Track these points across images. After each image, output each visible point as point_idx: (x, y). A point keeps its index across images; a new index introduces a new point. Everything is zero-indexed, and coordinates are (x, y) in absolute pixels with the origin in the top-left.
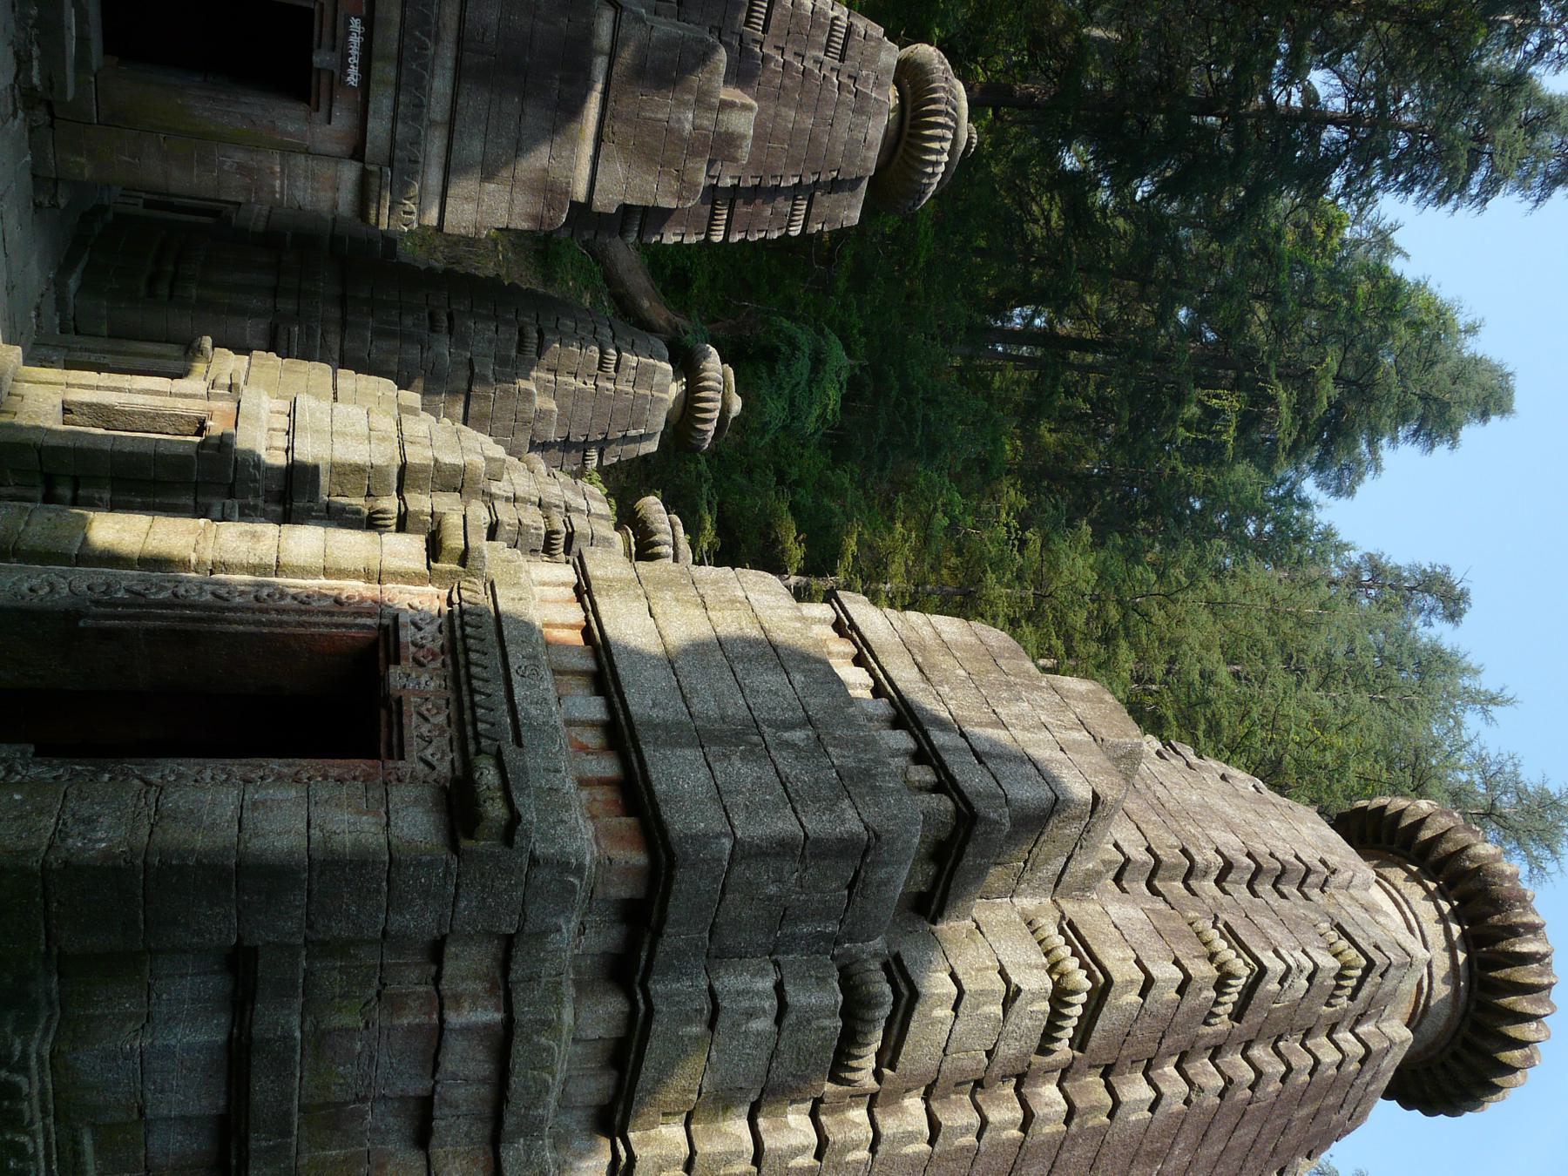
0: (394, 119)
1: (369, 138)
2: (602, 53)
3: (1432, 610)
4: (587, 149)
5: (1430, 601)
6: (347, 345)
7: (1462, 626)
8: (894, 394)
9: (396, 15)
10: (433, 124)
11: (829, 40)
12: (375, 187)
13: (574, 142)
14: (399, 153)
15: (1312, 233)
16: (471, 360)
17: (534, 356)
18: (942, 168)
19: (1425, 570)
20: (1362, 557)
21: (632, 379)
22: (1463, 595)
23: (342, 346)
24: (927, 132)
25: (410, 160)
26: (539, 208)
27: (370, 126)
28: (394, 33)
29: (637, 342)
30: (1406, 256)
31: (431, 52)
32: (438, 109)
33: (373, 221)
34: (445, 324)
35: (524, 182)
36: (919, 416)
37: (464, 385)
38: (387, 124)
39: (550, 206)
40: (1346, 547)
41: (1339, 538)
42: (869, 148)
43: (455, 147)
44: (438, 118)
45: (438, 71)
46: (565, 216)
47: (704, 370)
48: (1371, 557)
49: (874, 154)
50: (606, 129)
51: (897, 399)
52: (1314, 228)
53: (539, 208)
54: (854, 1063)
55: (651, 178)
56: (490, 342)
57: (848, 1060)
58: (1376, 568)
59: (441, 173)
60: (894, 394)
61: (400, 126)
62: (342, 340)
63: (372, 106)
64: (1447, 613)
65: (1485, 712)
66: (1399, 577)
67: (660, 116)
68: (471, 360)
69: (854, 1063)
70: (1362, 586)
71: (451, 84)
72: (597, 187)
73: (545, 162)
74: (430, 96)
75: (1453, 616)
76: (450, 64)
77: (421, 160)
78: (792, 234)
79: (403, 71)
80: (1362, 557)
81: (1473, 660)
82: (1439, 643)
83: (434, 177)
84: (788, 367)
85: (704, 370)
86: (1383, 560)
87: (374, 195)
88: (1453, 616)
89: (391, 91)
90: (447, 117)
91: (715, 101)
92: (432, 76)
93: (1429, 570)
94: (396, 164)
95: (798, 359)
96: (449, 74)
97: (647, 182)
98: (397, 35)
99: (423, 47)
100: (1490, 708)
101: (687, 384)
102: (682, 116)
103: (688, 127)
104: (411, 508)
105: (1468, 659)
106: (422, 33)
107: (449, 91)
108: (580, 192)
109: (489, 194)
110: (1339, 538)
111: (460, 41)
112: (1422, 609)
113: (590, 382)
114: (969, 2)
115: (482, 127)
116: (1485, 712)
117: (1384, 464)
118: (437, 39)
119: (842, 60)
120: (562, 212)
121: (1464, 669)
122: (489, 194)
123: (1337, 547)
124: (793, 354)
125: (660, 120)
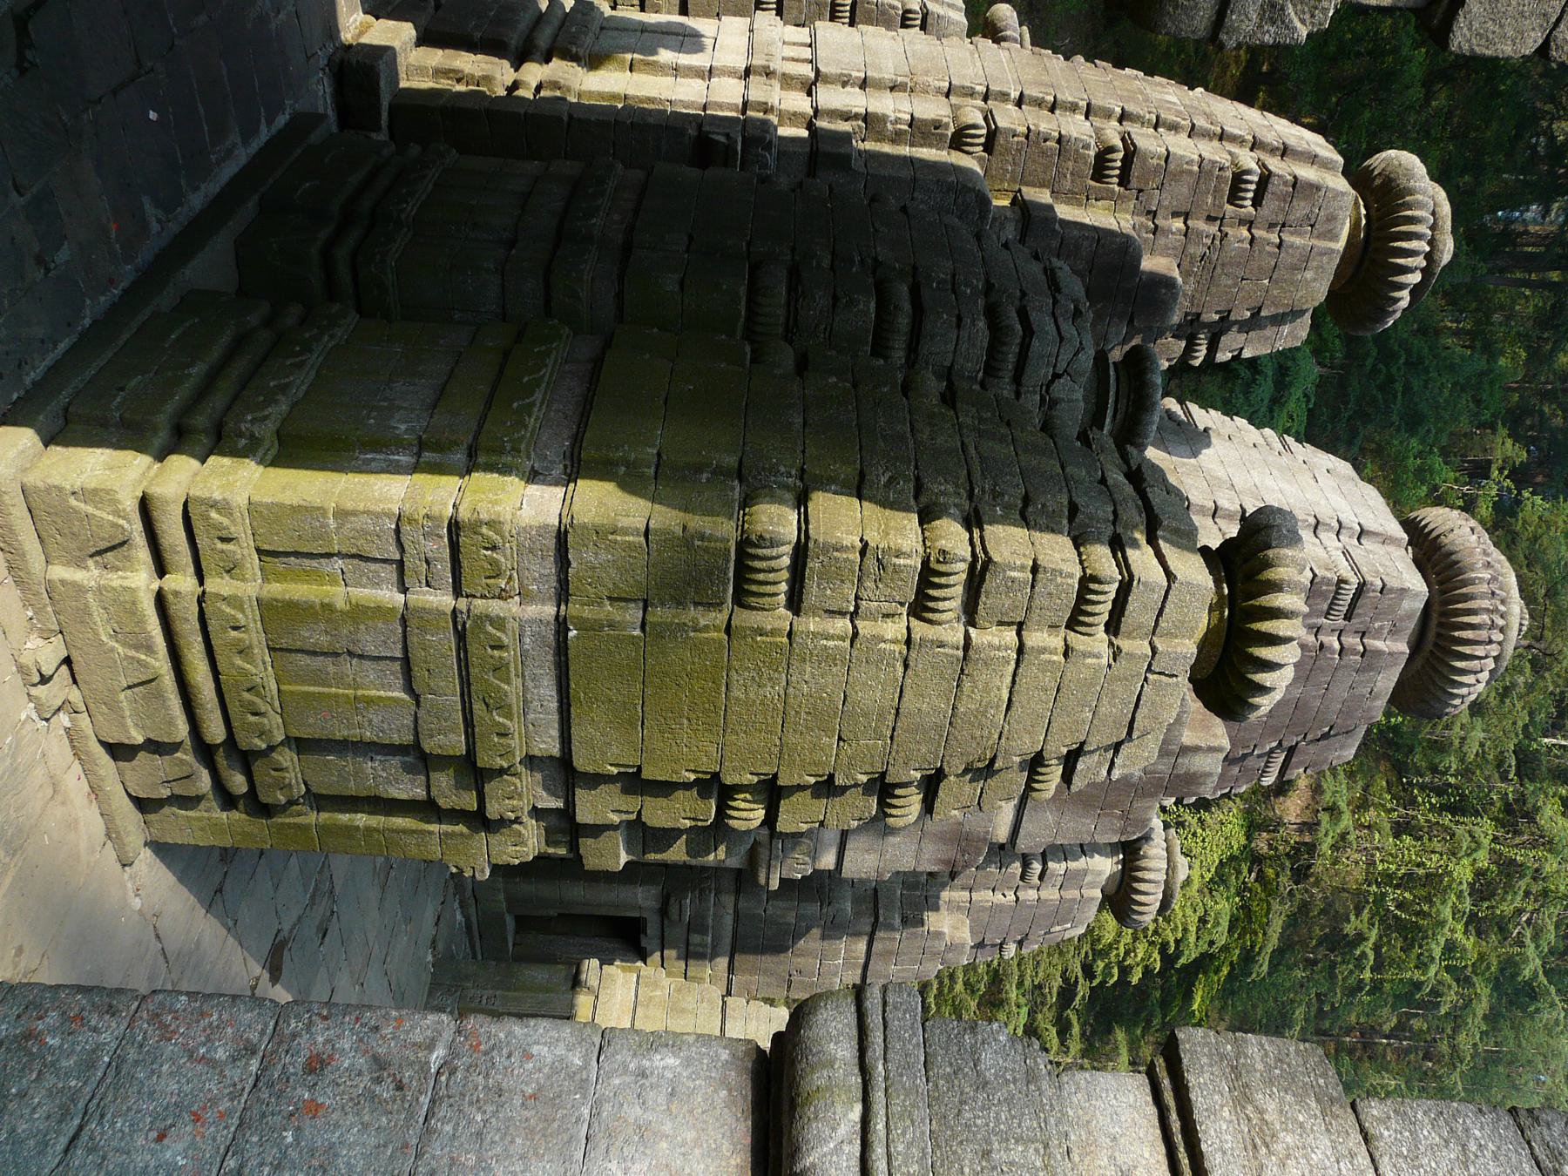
6: (740, 905)
8: (1369, 362)
11: (1330, 608)
17: (946, 879)
18: (1485, 676)
23: (736, 905)
24: (1456, 634)
33: (762, 881)
36: (1399, 387)
37: (868, 929)
42: (1376, 698)
47: (1144, 857)
51: (1374, 366)
60: (1369, 362)
62: (737, 900)
72: (1022, 832)
78: (1264, 784)
84: (1246, 393)
85: (1144, 857)
91: (1176, 748)
95: (1260, 385)
101: (1124, 862)
114: (1554, 728)
122: (894, 845)
124: (1254, 381)
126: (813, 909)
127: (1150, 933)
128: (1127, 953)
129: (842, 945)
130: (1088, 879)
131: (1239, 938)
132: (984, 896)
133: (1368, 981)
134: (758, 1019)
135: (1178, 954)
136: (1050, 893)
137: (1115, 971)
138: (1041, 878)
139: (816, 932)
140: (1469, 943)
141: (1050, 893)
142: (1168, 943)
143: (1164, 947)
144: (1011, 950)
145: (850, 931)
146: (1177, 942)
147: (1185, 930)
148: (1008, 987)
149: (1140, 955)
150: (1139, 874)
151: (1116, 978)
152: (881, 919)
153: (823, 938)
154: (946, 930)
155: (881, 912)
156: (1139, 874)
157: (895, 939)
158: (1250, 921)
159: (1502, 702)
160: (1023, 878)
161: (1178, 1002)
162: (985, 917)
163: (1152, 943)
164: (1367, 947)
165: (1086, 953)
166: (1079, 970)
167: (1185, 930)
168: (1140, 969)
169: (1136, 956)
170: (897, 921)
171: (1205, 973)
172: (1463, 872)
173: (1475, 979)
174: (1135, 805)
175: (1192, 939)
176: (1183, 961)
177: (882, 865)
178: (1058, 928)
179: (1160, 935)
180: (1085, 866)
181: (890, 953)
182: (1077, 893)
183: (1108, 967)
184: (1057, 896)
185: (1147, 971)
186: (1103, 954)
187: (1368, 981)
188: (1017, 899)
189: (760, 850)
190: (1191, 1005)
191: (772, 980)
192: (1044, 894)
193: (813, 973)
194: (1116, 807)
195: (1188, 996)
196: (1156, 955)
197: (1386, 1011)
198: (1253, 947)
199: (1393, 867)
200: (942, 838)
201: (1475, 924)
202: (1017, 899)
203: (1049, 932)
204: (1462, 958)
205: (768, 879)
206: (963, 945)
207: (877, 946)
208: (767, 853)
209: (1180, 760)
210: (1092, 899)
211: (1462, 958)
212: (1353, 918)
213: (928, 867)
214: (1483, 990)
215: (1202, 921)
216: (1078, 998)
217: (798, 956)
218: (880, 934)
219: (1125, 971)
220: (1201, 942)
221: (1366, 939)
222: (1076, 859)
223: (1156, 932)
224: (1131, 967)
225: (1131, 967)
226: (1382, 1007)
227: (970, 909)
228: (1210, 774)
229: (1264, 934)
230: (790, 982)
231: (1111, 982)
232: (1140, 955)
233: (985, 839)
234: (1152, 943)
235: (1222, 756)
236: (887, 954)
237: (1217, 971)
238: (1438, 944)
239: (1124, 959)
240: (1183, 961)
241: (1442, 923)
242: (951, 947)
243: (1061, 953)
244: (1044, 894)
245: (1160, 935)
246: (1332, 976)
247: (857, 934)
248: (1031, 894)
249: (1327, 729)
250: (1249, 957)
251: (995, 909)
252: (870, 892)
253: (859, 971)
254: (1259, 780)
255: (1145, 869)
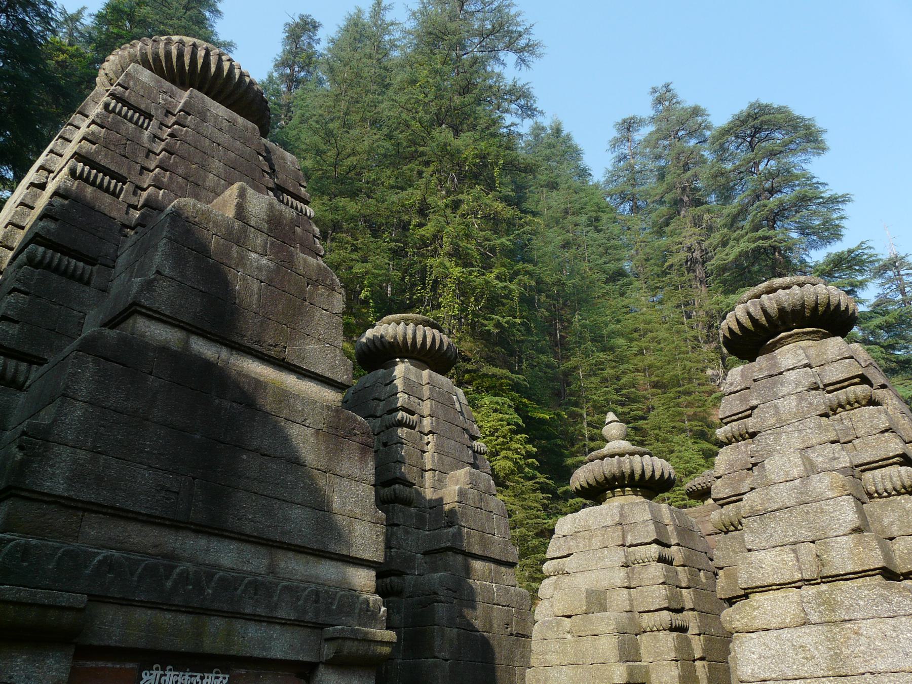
0: (271, 621)
1: (291, 656)
2: (187, 342)
3: (310, 38)
4: (291, 381)
5: (304, 38)
7: (322, 22)
9: (143, 616)
10: (272, 570)
12: (350, 647)
13: (284, 395)
14: (309, 617)
15: (62, 61)
16: (425, 554)
19: (287, 37)
20: (276, 71)
21: (417, 400)
22: (302, 18)
25: (317, 602)
26: (352, 447)
27: (279, 656)
28: (166, 619)
29: (377, 395)
30: (84, 8)
31: (192, 568)
32: (255, 562)
33: (386, 650)
34: (395, 579)
35: (330, 459)
37: (460, 558)
38: (276, 631)
39: (351, 434)
40: (270, 77)
41: (265, 80)
43: (299, 542)
44: (265, 562)
45: (211, 558)
46: (359, 418)
47: (395, 338)
48: (276, 66)
49: (240, 120)
50: (272, 353)
52: (60, 59)
53: (352, 447)
54: (747, 323)
55: (318, 314)
56: (407, 533)
57: (762, 326)
58: (283, 63)
59: (323, 562)
61: (281, 614)
63: (257, 653)
64: (312, 30)
65: (385, 9)
66: (290, 52)
67: (255, 288)
68: (425, 554)
69: (747, 323)
70: (293, 74)
71: (227, 542)
72: (328, 374)
73: (309, 431)
74: (245, 572)
75: (315, 26)
76: (203, 542)
77: (313, 587)
79: (216, 606)
80: (276, 71)
81: (353, 11)
82: (343, 27)
83: (328, 571)
85: (395, 338)
86: (279, 59)
87: (362, 648)
88: (315, 26)
89: (238, 625)
90: (263, 551)
91: (237, 224)
92: (219, 567)
93: (287, 34)
94: (322, 619)
96: (216, 544)
97: (321, 319)
98: (168, 616)
99: (184, 577)
100: (383, 5)
102: (255, 264)
103: (264, 261)
104: (880, 565)
105: (352, 14)
106: (167, 578)
107: (234, 546)
108: (331, 396)
109: (344, 504)
110: (265, 80)
111: (176, 525)
112: (309, 43)
113: (426, 439)
115: (277, 504)
116: (385, 9)
117: (229, 40)
118: (173, 557)
119: (149, 117)
120: (356, 420)
121: (358, 16)
122: (344, 504)
123: (270, 82)
125: (260, 289)
126: (441, 609)
127: (505, 440)
128: (518, 453)
129: (476, 583)
130: (412, 378)
131: (505, 393)
132: (429, 460)
133: (522, 320)
134: (545, 653)
135: (517, 424)
136: (426, 407)
137: (530, 460)
138: (412, 413)
139: (467, 612)
140: (496, 271)
141: (426, 407)
142: (510, 429)
143: (516, 432)
144: (479, 444)
145: (463, 574)
146: (509, 424)
147: (501, 420)
148: (546, 526)
149: (519, 446)
150: (409, 341)
151: (534, 460)
152: (449, 544)
153: (474, 608)
154: (457, 487)
155: (443, 545)
156: (409, 341)
157: (467, 532)
158: (495, 387)
159: (360, 249)
160: (413, 427)
161: (546, 427)
162: (447, 460)
163: (511, 439)
164: (503, 321)
165: (520, 477)
166: (531, 483)
167: (501, 420)
168: (527, 446)
169: (520, 448)
170: (451, 530)
171: (528, 412)
172: (456, 271)
173: (515, 268)
174: (302, 271)
175: (507, 416)
176: (520, 422)
177: (367, 518)
178: (457, 405)
179: (506, 435)
180: (401, 380)
181: (482, 539)
182: (425, 388)
183: (528, 465)
184: (428, 402)
185: (529, 441)
186: (520, 469)
187: (522, 320)
188: (430, 432)
189: (345, 652)
190: (547, 420)
191: (518, 652)
192: (426, 412)
193: (507, 612)
194: (303, 291)
195: (542, 421)
196: (519, 436)
197: (538, 314)
198: (510, 385)
199: (456, 306)
200: (335, 452)
201: (487, 267)
202: (430, 432)
203: (461, 413)
204: (505, 275)
205: (383, 643)
206: (471, 474)
207: (476, 549)
208: (348, 644)
209: (253, 223)
210: (430, 376)
211: (505, 275)
212: (487, 328)
213: (369, 470)
214: (520, 266)
215: (495, 411)
216: (547, 481)
217: (491, 626)
218: (465, 546)
219: (529, 455)
220: (509, 412)
221: (498, 320)
222: (397, 387)
223: (504, 437)
224: (527, 452)
225: (527, 452)
226: (536, 316)
227: (441, 472)
228: (271, 205)
229: (502, 378)
230: (518, 635)
231: (537, 463)
232: (519, 446)
233: (337, 410)
234: (511, 439)
235: (250, 191)
236: (483, 542)
237: (526, 405)
238: (497, 284)
239: (522, 455)
240: (520, 422)
241: (487, 282)
242: (474, 484)
243: (523, 493)
244: (426, 412)
245: (506, 435)
246: (522, 341)
247: (468, 570)
248: (427, 423)
249: (261, 158)
250: (516, 387)
251: (439, 450)
252: (427, 559)
253: (503, 569)
254: (309, 218)
255: (405, 337)
